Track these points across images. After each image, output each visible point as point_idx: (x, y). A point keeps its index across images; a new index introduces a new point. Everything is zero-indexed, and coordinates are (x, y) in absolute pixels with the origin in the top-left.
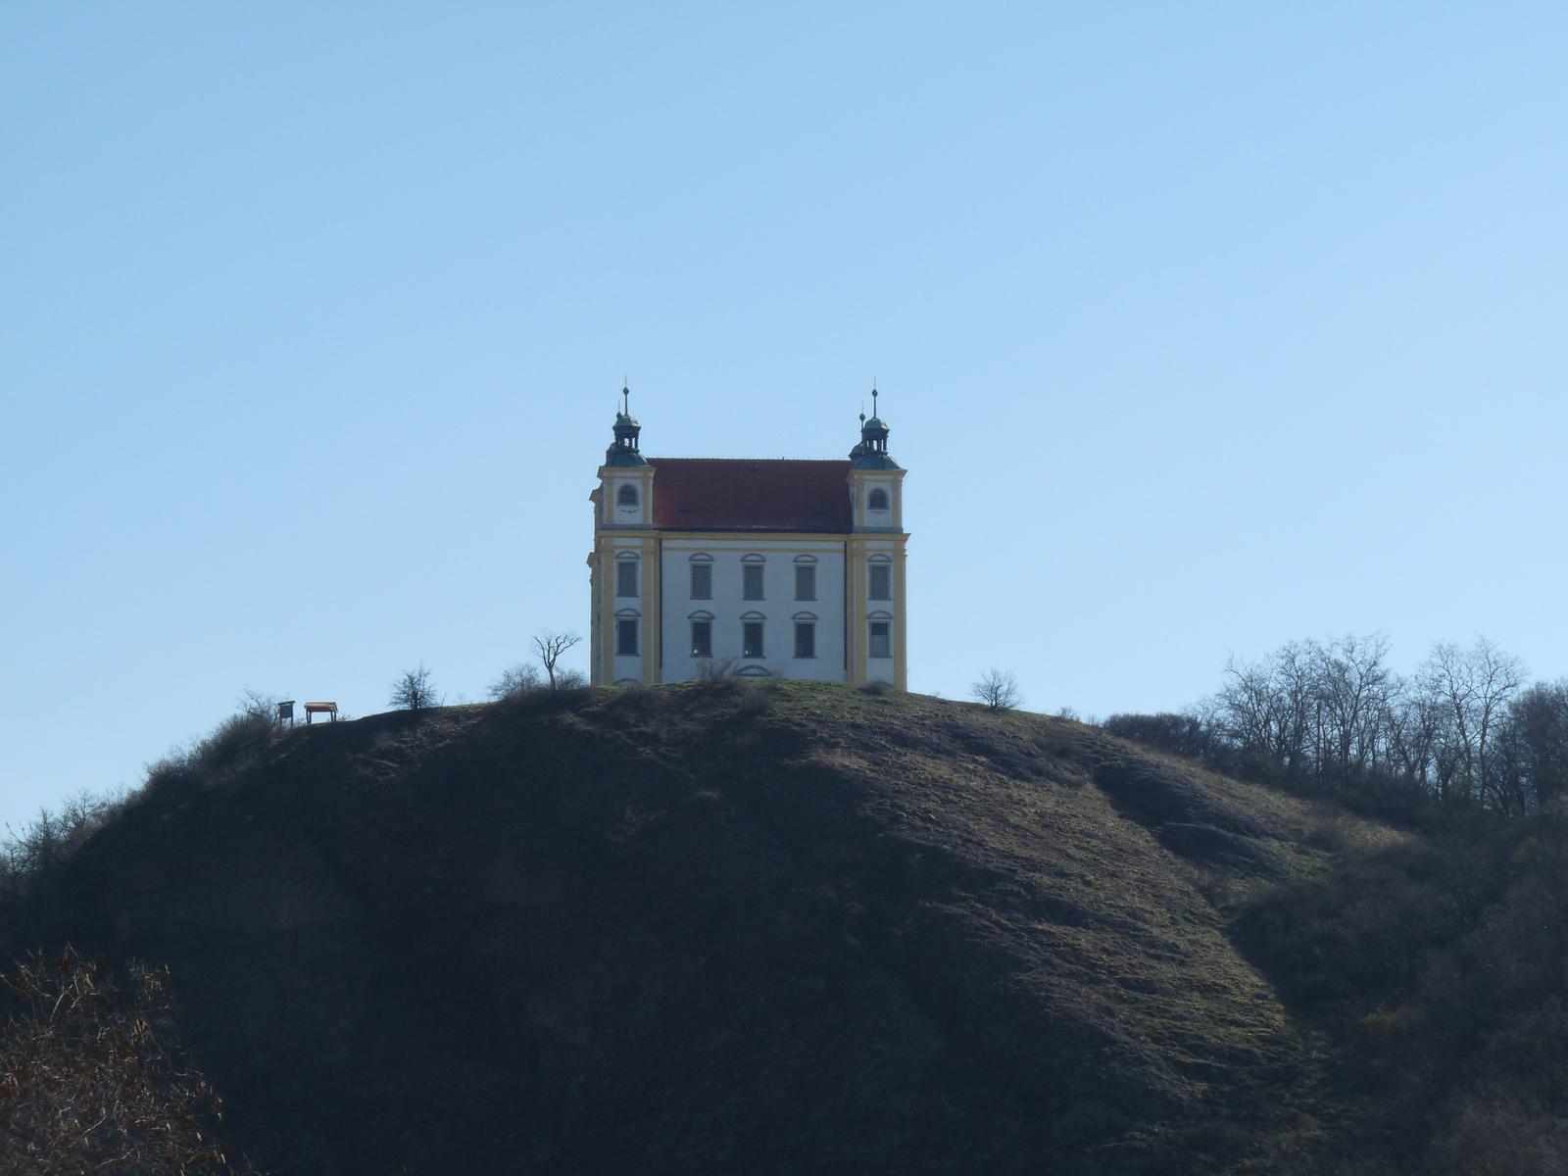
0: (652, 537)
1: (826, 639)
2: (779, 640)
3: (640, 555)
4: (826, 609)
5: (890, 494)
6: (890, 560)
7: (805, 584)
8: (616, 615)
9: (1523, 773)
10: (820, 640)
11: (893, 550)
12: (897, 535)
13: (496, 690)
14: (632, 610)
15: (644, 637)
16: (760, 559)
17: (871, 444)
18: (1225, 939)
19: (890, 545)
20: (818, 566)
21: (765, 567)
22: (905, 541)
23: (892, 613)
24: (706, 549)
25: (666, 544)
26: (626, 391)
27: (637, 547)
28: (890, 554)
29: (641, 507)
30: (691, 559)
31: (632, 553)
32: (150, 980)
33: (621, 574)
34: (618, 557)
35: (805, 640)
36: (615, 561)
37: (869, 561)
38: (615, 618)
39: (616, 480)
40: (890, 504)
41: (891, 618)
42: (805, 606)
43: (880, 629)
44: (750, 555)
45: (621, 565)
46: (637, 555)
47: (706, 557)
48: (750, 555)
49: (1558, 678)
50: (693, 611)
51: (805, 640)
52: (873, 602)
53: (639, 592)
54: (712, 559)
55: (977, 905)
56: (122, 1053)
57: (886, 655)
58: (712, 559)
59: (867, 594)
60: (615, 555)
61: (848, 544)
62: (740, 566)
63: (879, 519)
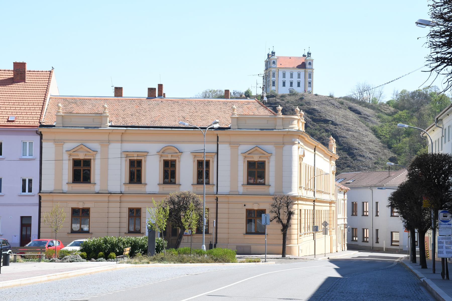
1: (302, 84)
2: (295, 84)
4: (302, 80)
5: (276, 62)
7: (299, 76)
10: (286, 84)
12: (312, 69)
18: (341, 196)
19: (311, 70)
20: (301, 73)
25: (279, 70)
30: (290, 72)
33: (309, 76)
35: (299, 85)
40: (312, 64)
42: (299, 79)
43: (310, 83)
51: (299, 85)
52: (309, 79)
53: (275, 77)
55: (132, 177)
56: (435, 160)
57: (311, 87)
62: (290, 73)
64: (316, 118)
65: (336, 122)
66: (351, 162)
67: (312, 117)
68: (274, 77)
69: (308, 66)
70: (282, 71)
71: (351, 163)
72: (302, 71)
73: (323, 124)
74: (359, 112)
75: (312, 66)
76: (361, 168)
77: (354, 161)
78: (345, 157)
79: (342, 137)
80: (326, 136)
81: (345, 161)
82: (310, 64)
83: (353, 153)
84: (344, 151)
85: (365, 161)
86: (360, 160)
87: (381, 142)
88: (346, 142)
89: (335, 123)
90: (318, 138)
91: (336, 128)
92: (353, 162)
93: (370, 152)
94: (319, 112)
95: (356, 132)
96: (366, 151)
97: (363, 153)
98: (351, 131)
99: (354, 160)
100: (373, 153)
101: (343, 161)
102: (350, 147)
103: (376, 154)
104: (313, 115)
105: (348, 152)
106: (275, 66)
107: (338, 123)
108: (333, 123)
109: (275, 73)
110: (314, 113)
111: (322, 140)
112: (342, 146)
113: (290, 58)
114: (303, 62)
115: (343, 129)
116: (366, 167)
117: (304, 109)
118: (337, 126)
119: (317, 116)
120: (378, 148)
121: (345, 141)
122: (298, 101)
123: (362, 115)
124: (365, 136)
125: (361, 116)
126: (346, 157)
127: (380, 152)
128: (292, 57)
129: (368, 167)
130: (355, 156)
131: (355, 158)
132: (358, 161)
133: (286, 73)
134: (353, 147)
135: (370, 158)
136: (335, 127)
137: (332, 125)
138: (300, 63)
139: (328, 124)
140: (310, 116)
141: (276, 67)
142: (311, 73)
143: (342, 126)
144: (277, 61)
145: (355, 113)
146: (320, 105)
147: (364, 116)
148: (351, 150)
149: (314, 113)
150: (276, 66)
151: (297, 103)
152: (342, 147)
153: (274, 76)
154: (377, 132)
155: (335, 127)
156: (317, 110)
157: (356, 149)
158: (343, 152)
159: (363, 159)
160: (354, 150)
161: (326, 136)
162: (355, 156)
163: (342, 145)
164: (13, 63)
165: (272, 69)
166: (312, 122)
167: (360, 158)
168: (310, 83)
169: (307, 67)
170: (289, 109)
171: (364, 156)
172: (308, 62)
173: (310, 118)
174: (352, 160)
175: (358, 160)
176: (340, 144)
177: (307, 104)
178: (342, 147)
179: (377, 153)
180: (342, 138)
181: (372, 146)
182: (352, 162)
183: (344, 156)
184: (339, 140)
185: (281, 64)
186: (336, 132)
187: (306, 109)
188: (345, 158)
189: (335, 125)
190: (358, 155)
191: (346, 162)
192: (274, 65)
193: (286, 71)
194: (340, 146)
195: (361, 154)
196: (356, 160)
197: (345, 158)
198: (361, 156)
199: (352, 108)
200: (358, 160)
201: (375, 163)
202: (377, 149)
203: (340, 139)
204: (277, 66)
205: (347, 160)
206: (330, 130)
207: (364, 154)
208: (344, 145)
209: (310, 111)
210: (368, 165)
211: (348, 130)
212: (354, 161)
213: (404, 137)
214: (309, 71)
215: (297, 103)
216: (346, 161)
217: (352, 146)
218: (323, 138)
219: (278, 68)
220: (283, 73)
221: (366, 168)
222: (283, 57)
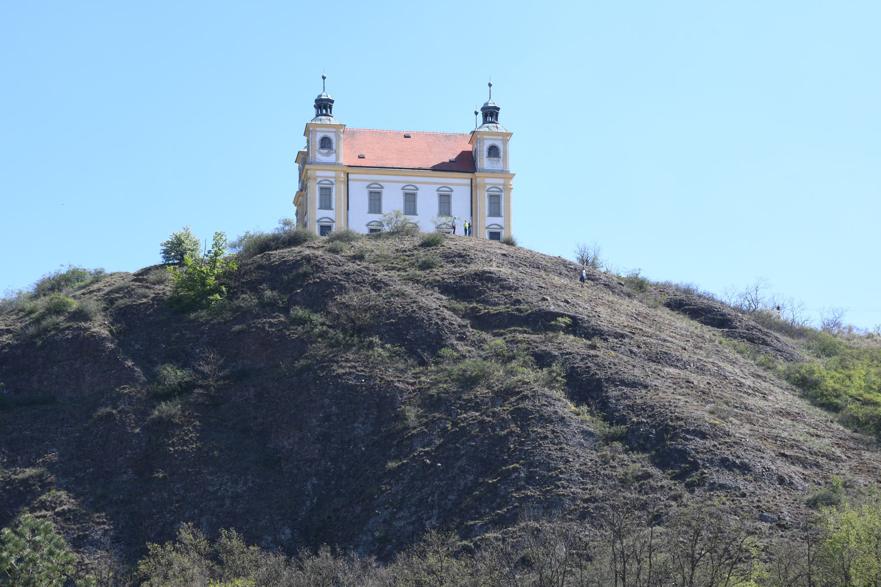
0: (342, 171)
3: (334, 182)
6: (501, 191)
7: (445, 201)
8: (318, 221)
9: (286, 372)
11: (335, 177)
12: (506, 175)
14: (498, 225)
19: (501, 181)
20: (418, 192)
22: (511, 178)
23: (333, 218)
25: (350, 176)
26: (490, 85)
28: (333, 180)
30: (368, 187)
33: (321, 195)
34: (319, 183)
36: (486, 194)
38: (317, 224)
39: (318, 133)
40: (501, 154)
41: (502, 228)
45: (491, 196)
46: (331, 182)
47: (448, 190)
48: (491, 188)
50: (369, 221)
53: (333, 206)
58: (382, 187)
59: (487, 213)
63: (496, 165)
64: (492, 310)
65: (593, 323)
66: (675, 498)
67: (473, 309)
68: (329, 207)
69: (484, 162)
70: (369, 183)
71: (673, 503)
72: (458, 184)
73: (525, 332)
74: (723, 315)
75: (505, 161)
76: (732, 523)
77: (692, 492)
78: (640, 473)
79: (623, 383)
80: (535, 381)
81: (640, 492)
82: (493, 152)
83: (683, 454)
84: (632, 449)
85: (752, 489)
86: (722, 487)
87: (845, 423)
88: (645, 403)
90: (493, 392)
91: (594, 347)
92: (687, 495)
93: (783, 455)
94: (510, 288)
95: (701, 370)
96: (757, 444)
97: (740, 452)
98: (676, 367)
99: (690, 487)
100: (798, 458)
101: (628, 495)
102: (667, 425)
103: (817, 465)
104: (478, 302)
105: (653, 453)
106: (332, 158)
107: (606, 329)
108: (576, 327)
109: (503, 194)
110: (481, 293)
111: (513, 399)
112: (625, 424)
114: (463, 152)
115: (631, 352)
116: (762, 518)
117: (438, 278)
119: (499, 304)
120: (827, 441)
121: (639, 401)
122: (408, 253)
124: (750, 391)
126: (648, 476)
127: (837, 459)
128: (418, 134)
129: (773, 520)
130: (695, 466)
131: (695, 477)
132: (711, 490)
134: (680, 423)
135: (781, 480)
136: (589, 342)
137: (572, 337)
138: (450, 155)
139: (551, 334)
140: (461, 306)
141: (335, 164)
142: (501, 191)
143: (626, 340)
144: (338, 138)
145: (702, 322)
148: (671, 439)
149: (481, 293)
150: (338, 158)
151: (404, 260)
152: (621, 429)
153: (326, 204)
154: (816, 384)
155: (589, 342)
156: (500, 279)
157: (703, 436)
158: (626, 452)
159: (741, 483)
160: (687, 440)
161: (541, 382)
162: (695, 466)
163: (622, 420)
165: (319, 173)
166: (471, 330)
167: (726, 478)
169: (479, 165)
170: (357, 283)
171: (745, 468)
172: (487, 144)
173: (463, 317)
174: (680, 488)
175: (713, 487)
176: (612, 414)
177: (453, 262)
178: (621, 429)
179: (822, 461)
180: (625, 389)
181: (785, 429)
182: (680, 496)
183: (636, 468)
184: (608, 398)
185: (361, 157)
186: (590, 364)
187: (443, 279)
188: (638, 478)
189: (588, 336)
190: (711, 462)
191: (645, 497)
192: (328, 155)
194: (611, 425)
195: (730, 457)
196: (698, 485)
197: (638, 481)
198: (726, 464)
199: (687, 304)
200: (713, 487)
201: (813, 504)
202: (823, 444)
203: (613, 392)
204: (343, 161)
205: (651, 488)
206: (562, 354)
207: (748, 458)
208: (635, 419)
210: (768, 510)
211: (659, 358)
212: (692, 492)
214: (488, 182)
215: (404, 260)
216: (646, 493)
217: (678, 418)
218: (519, 393)
219: (349, 170)
221: (759, 524)
222: (373, 132)
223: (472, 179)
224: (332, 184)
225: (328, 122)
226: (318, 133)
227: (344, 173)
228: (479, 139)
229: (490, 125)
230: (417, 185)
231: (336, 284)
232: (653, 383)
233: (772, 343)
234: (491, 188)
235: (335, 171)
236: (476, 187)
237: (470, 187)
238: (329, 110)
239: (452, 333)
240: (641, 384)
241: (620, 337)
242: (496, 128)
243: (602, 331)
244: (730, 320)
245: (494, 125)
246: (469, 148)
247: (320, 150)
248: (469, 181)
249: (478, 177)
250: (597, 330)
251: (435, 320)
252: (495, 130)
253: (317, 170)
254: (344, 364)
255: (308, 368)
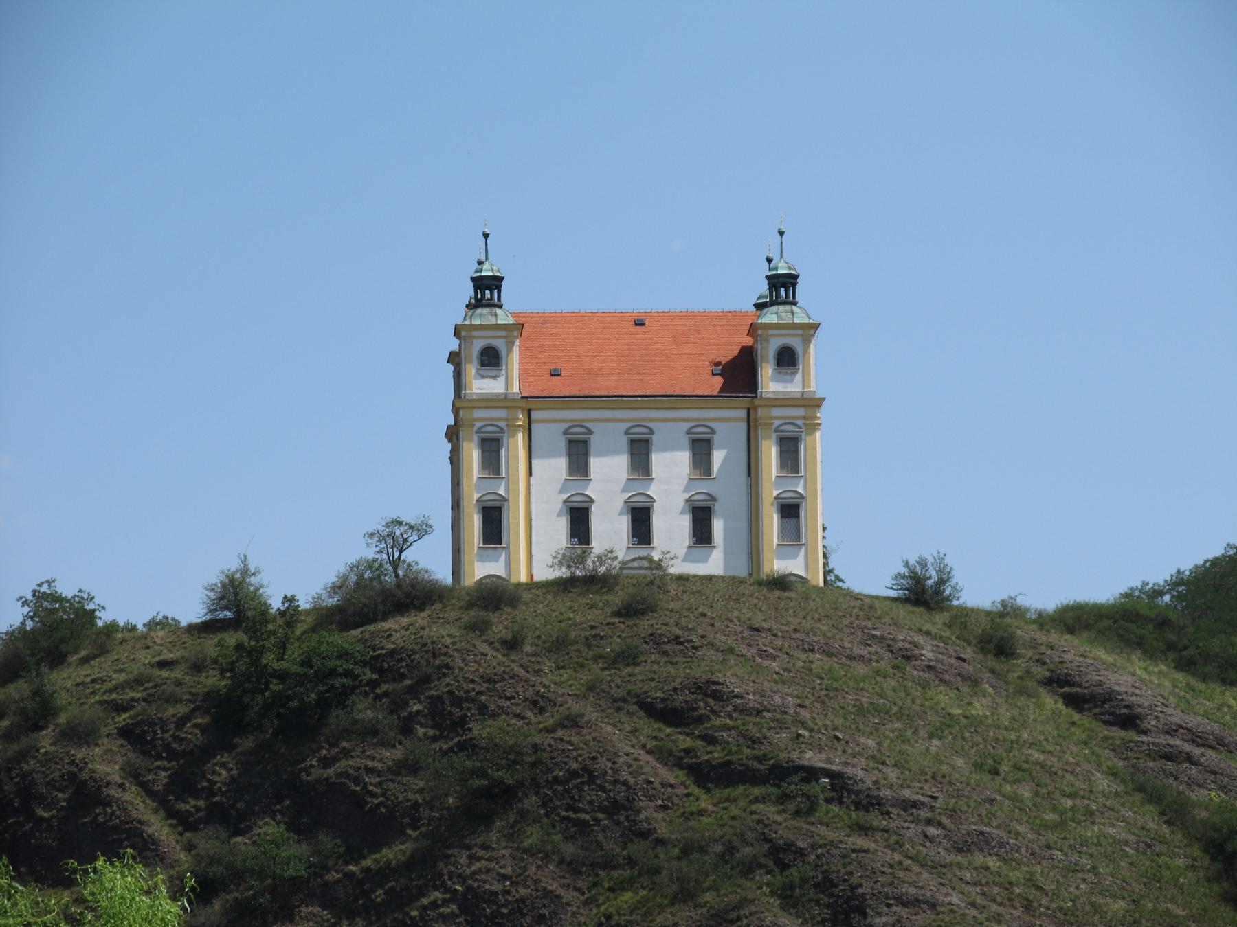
3: (505, 429)
5: (799, 351)
13: (335, 589)
15: (474, 524)
16: (646, 430)
17: (483, 295)
21: (653, 439)
22: (819, 406)
24: (583, 420)
27: (501, 419)
28: (502, 424)
29: (504, 372)
30: (566, 432)
31: (704, 426)
32: (373, 897)
34: (776, 431)
37: (776, 431)
39: (475, 341)
44: (786, 424)
46: (501, 429)
48: (786, 424)
49: (202, 606)
51: (702, 533)
54: (590, 432)
58: (590, 432)
60: (475, 429)
61: (751, 411)
70: (565, 426)
79: (902, 901)
89: (860, 791)
113: (640, 323)
118: (874, 819)
123: (1145, 732)
125: (1144, 738)
133: (592, 437)
146: (774, 658)
147: (1163, 740)
164: (471, 284)
168: (790, 511)
177: (665, 653)
185: (555, 374)
193: (713, 425)
209: (680, 700)
213: (914, 733)
219: (532, 404)
220: (570, 442)
223: (749, 410)
224: (502, 431)
225: (492, 321)
226: (475, 341)
227: (523, 410)
228: (761, 336)
229: (782, 308)
230: (651, 425)
231: (473, 700)
232: (947, 900)
233: (1202, 760)
234: (781, 425)
235: (506, 407)
236: (756, 427)
237: (746, 424)
238: (496, 292)
239: (651, 798)
240: (926, 902)
241: (912, 807)
242: (789, 315)
243: (882, 799)
244: (1139, 717)
245: (788, 307)
246: (748, 341)
247: (480, 372)
248: (742, 414)
249: (760, 406)
250: (874, 797)
251: (624, 776)
252: (787, 319)
253: (474, 407)
254: (480, 853)
255: (471, 739)
